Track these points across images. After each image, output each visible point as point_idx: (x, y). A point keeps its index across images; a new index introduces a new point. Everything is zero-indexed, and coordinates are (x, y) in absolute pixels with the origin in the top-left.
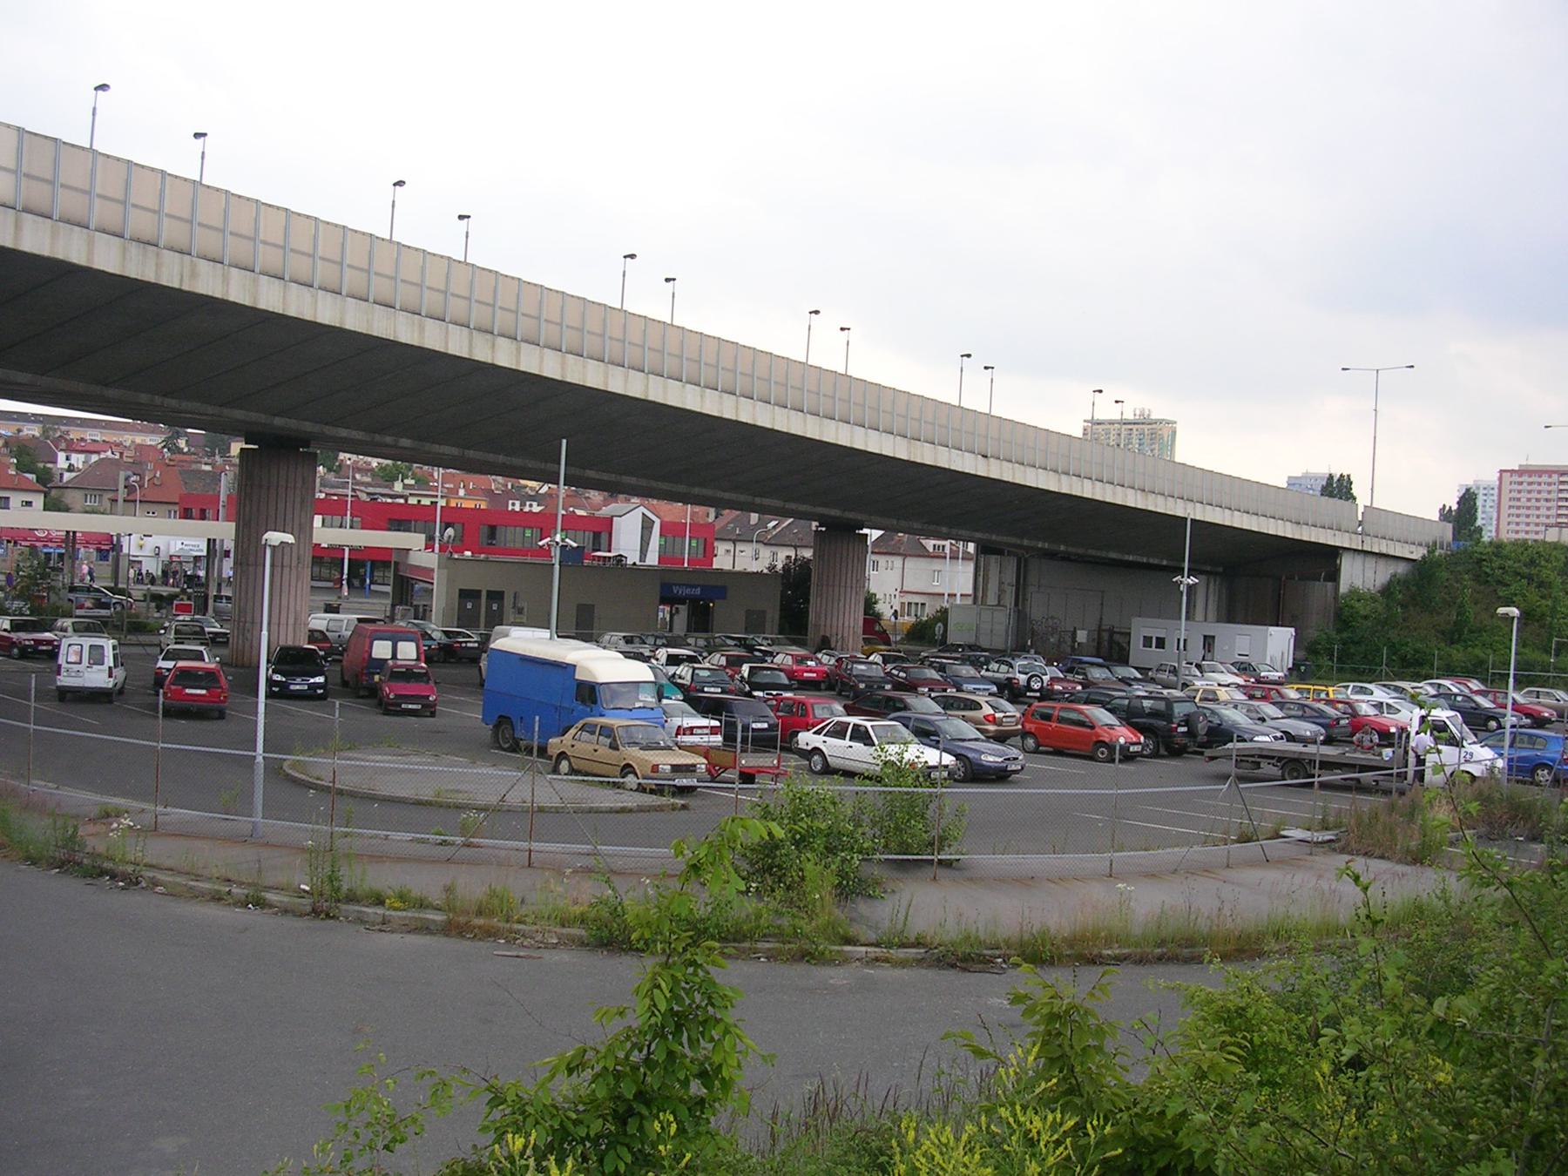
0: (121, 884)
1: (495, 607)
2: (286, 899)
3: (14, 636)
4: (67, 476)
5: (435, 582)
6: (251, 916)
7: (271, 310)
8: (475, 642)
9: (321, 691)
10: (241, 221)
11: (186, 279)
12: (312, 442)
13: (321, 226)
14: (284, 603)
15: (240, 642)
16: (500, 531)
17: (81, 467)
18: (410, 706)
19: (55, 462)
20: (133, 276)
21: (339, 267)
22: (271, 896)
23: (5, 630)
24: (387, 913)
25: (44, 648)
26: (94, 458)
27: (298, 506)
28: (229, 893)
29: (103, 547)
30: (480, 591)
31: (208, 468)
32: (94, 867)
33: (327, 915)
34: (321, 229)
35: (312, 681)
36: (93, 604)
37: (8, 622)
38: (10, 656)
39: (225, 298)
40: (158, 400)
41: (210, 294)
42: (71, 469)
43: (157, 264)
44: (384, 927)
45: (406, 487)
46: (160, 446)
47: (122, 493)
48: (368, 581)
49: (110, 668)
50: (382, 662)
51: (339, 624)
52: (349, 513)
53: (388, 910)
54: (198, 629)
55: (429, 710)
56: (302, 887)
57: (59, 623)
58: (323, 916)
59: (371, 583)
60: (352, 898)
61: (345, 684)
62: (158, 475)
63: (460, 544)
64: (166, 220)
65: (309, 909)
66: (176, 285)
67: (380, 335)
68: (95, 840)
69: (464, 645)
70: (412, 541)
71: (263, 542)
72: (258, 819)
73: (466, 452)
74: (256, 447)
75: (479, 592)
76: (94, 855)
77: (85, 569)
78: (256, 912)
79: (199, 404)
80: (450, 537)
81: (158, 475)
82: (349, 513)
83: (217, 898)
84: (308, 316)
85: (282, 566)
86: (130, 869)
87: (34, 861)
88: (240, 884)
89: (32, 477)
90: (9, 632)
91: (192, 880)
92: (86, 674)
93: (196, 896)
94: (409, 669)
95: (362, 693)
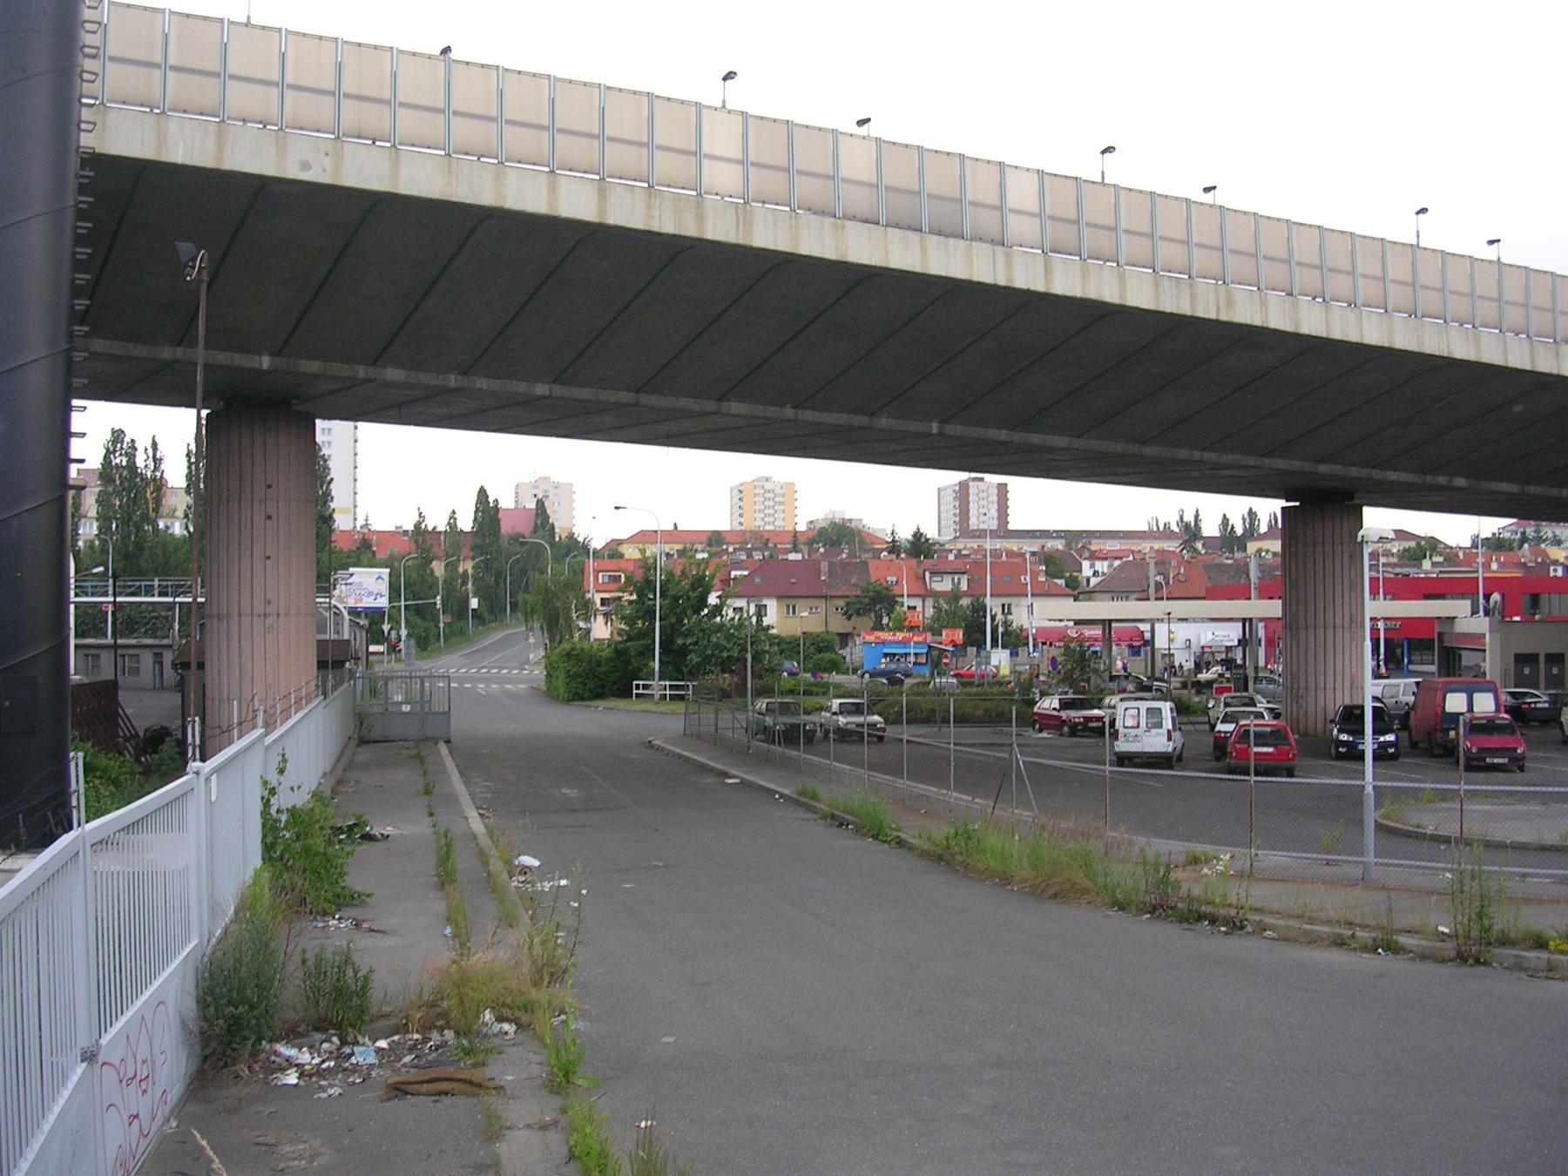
0: (1223, 929)
1: (1555, 671)
2: (1425, 943)
3: (1064, 714)
4: (1093, 581)
5: (1487, 648)
6: (1383, 960)
7: (1314, 334)
8: (1545, 702)
9: (1393, 750)
10: (1273, 245)
11: (1222, 308)
12: (1356, 495)
13: (1358, 241)
14: (1339, 666)
15: (1295, 711)
16: (1544, 600)
17: (1106, 571)
18: (1496, 761)
19: (1081, 571)
20: (1168, 310)
21: (1381, 284)
22: (1403, 940)
23: (1054, 709)
24: (1554, 957)
25: (1094, 725)
26: (1117, 563)
27: (1346, 560)
28: (1353, 936)
29: (1134, 644)
30: (1537, 655)
31: (1230, 562)
32: (1189, 910)
33: (1478, 962)
34: (1357, 243)
35: (1382, 739)
36: (1136, 688)
37: (1057, 701)
38: (1061, 735)
39: (1265, 325)
40: (1197, 455)
41: (1249, 322)
42: (1096, 574)
43: (1191, 296)
44: (1551, 974)
45: (1434, 564)
46: (1178, 550)
47: (1152, 590)
48: (1406, 660)
49: (1169, 731)
50: (1455, 717)
51: (1396, 688)
52: (1381, 590)
53: (1553, 953)
54: (1247, 700)
55: (1518, 764)
56: (1441, 929)
57: (1107, 701)
58: (1471, 961)
59: (1409, 663)
60: (1505, 941)
61: (1414, 745)
62: (1182, 571)
63: (1505, 610)
64: (1196, 251)
65: (1453, 954)
66: (1213, 316)
67: (1433, 353)
68: (1189, 884)
69: (1533, 706)
70: (1457, 608)
71: (1359, 539)
72: (1370, 858)
73: (1527, 488)
74: (1297, 504)
75: (1537, 655)
76: (1190, 899)
77: (1119, 664)
78: (1388, 958)
79: (1239, 456)
80: (1496, 602)
81: (1182, 571)
82: (1381, 590)
83: (1339, 943)
84: (1353, 337)
85: (1334, 627)
86: (1233, 912)
87: (1122, 907)
88: (1364, 927)
89: (1061, 582)
90: (1059, 711)
91: (1307, 923)
92: (1145, 739)
93: (1312, 940)
94: (1490, 720)
95: (1436, 751)
